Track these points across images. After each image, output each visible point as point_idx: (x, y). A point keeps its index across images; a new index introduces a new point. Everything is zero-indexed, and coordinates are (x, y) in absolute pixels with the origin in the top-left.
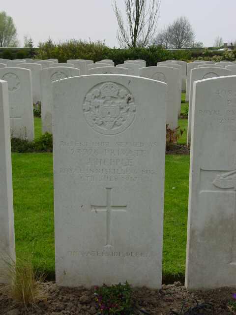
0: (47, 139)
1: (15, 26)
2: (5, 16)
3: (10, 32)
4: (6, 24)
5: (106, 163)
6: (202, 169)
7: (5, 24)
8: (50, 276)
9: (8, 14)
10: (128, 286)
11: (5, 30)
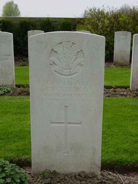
0: (21, 60)
1: (20, 10)
2: (13, 4)
3: (16, 14)
4: (14, 9)
5: (82, 96)
6: (52, 122)
7: (13, 9)
8: (26, 164)
9: (15, 3)
10: (101, 13)
11: (13, 13)
